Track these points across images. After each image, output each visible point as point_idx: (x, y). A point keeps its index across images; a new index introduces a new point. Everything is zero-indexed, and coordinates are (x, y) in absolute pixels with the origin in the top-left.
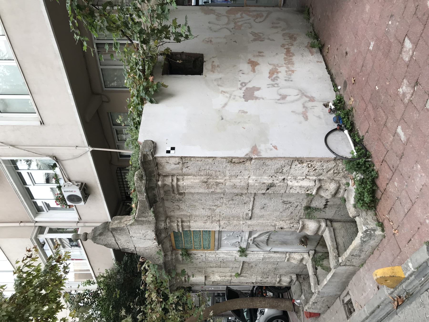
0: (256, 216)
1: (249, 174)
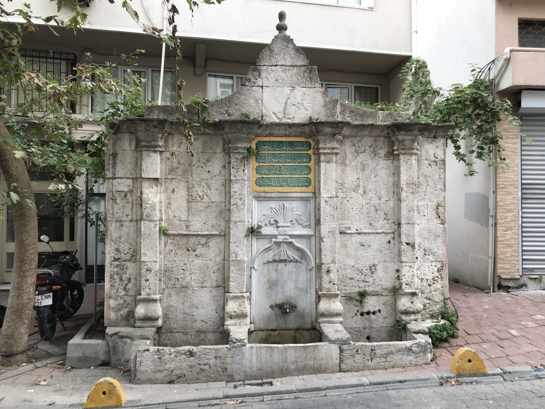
0: (345, 239)
1: (421, 223)
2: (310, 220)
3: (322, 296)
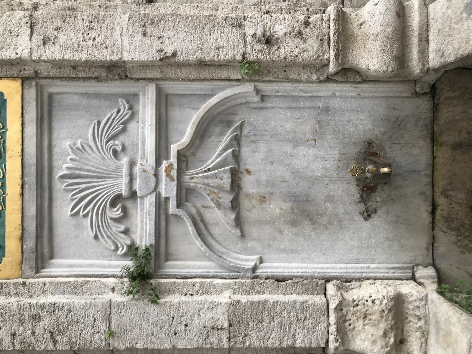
2: (111, 97)
3: (343, 63)
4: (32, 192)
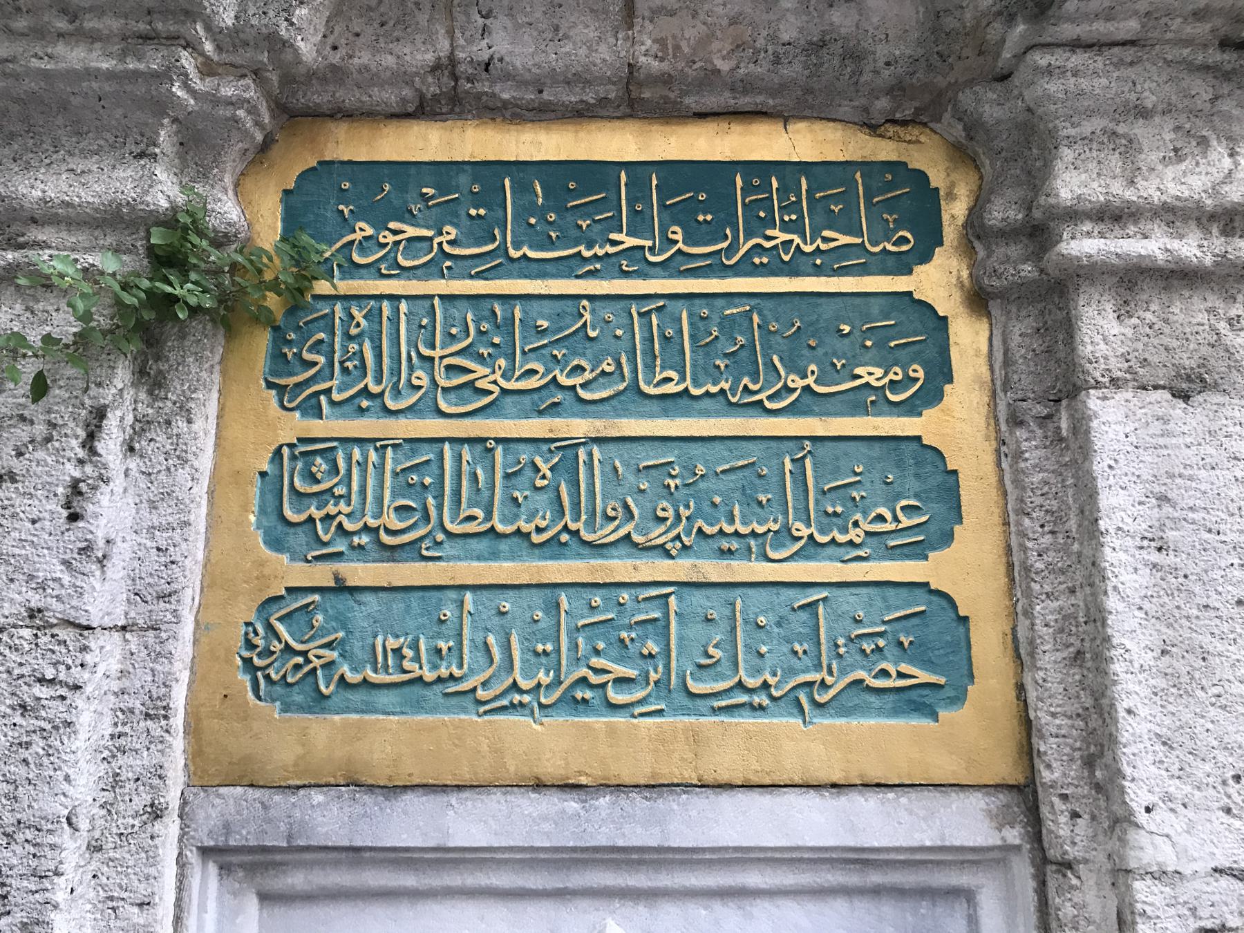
4: (547, 827)
